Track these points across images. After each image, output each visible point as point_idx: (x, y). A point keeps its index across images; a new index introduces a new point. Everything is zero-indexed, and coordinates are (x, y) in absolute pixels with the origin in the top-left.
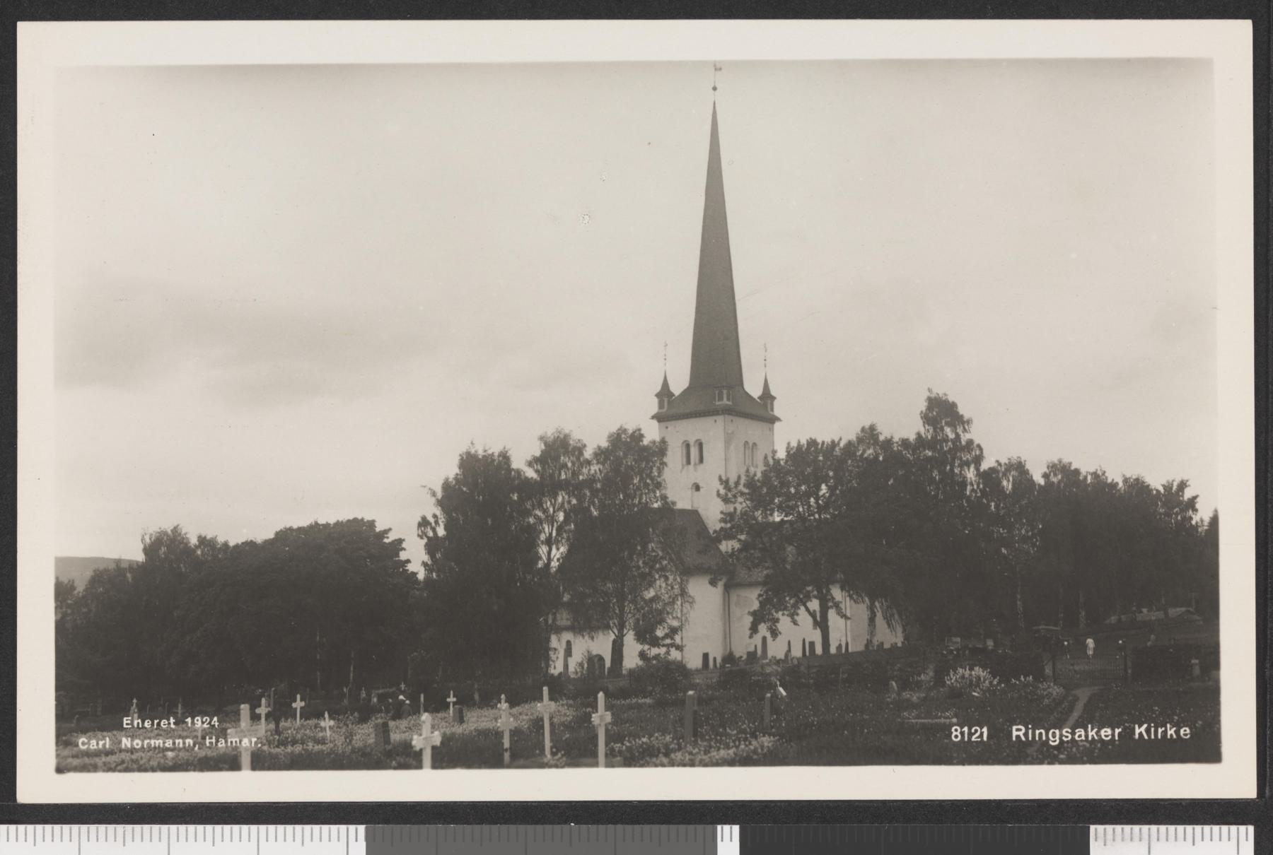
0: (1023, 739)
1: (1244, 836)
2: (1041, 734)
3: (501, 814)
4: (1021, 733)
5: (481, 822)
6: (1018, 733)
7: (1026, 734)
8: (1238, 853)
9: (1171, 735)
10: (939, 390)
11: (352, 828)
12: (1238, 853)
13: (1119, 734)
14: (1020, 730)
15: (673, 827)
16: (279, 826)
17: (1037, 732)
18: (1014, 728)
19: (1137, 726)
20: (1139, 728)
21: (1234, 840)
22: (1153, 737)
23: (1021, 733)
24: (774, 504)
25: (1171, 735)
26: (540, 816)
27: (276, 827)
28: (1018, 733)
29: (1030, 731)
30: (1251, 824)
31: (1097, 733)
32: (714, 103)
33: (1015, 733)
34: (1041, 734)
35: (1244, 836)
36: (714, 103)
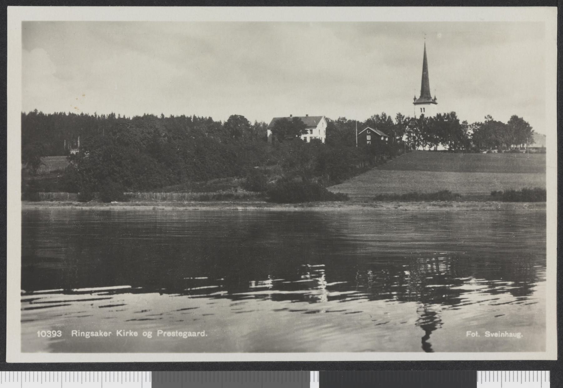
0: (77, 335)
1: (546, 374)
2: (83, 334)
3: (214, 367)
4: (76, 333)
5: (205, 370)
6: (74, 333)
7: (77, 334)
8: (22, 387)
9: (119, 335)
10: (37, 109)
11: (543, 372)
12: (22, 387)
13: (110, 334)
14: (75, 332)
15: (292, 372)
16: (59, 372)
17: (82, 333)
18: (73, 331)
19: (117, 331)
20: (119, 331)
21: (120, 380)
22: (124, 335)
23: (76, 333)
24: (417, 271)
25: (119, 335)
26: (231, 368)
27: (70, 372)
28: (74, 333)
29: (79, 333)
30: (151, 371)
31: (133, 334)
32: (425, 44)
33: (73, 334)
34: (83, 334)
35: (546, 374)
36: (425, 44)
